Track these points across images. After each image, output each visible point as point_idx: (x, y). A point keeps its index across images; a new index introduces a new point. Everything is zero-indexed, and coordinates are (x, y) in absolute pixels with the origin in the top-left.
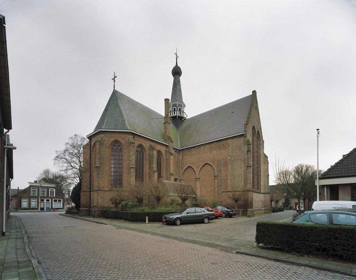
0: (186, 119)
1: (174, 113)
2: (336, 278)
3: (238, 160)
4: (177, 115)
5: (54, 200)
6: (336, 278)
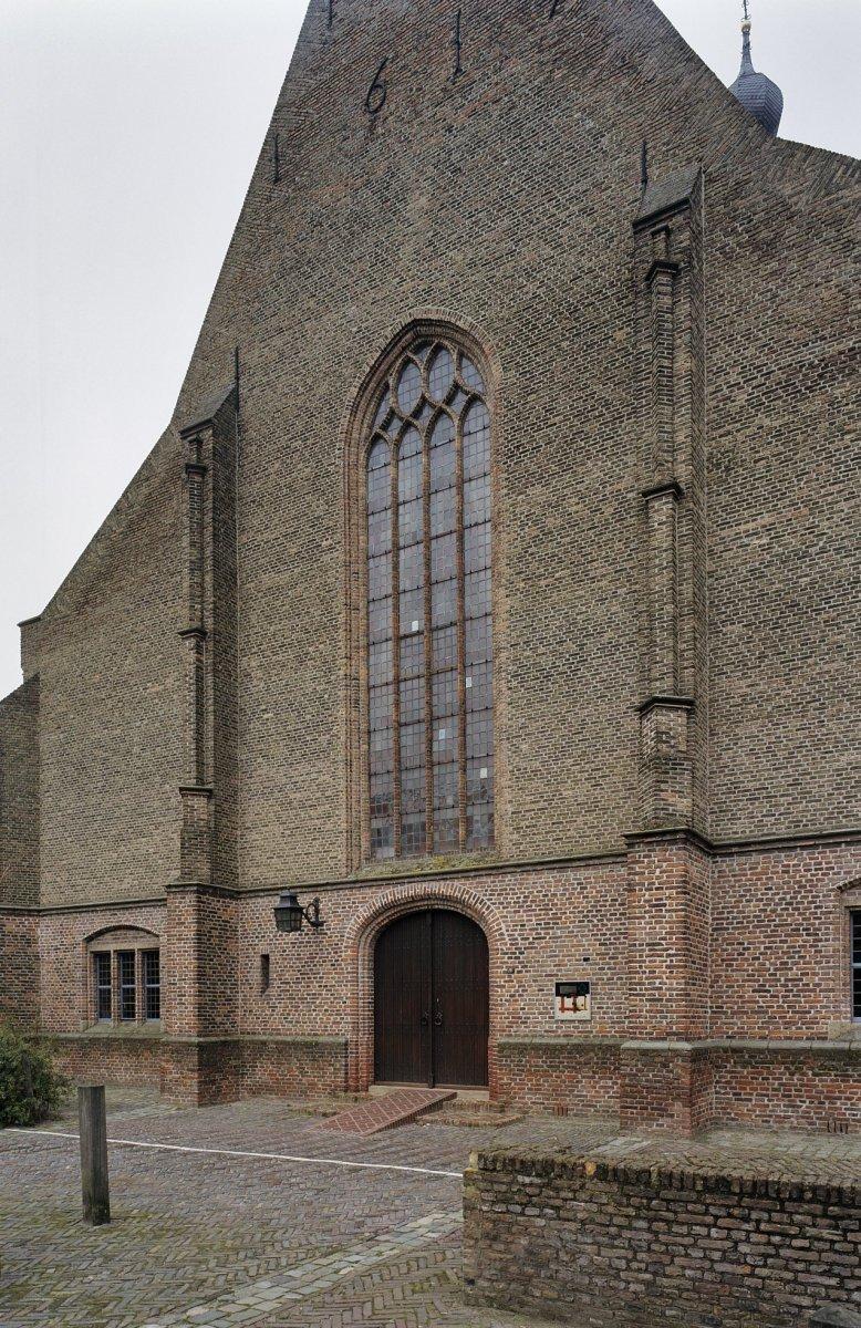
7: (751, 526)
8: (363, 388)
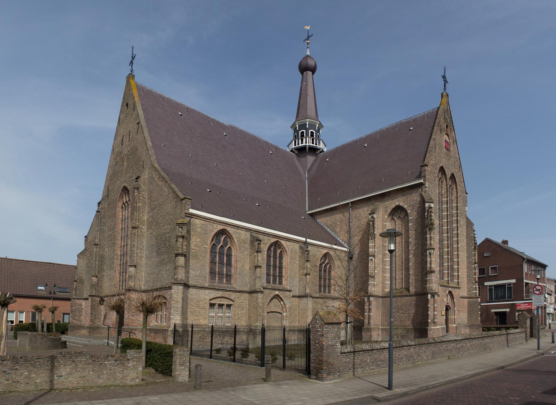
0: (323, 151)
1: (302, 140)
2: (448, 108)
3: (255, 241)
4: (307, 144)
5: (491, 268)
6: (448, 108)
7: (149, 232)
8: (120, 197)
